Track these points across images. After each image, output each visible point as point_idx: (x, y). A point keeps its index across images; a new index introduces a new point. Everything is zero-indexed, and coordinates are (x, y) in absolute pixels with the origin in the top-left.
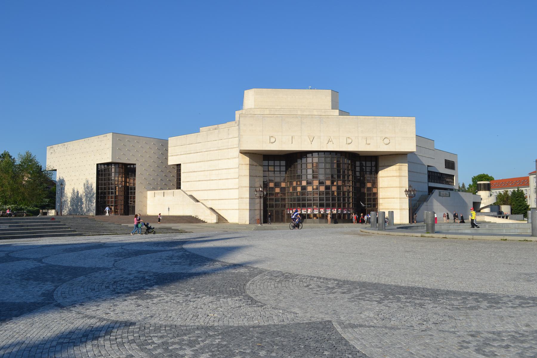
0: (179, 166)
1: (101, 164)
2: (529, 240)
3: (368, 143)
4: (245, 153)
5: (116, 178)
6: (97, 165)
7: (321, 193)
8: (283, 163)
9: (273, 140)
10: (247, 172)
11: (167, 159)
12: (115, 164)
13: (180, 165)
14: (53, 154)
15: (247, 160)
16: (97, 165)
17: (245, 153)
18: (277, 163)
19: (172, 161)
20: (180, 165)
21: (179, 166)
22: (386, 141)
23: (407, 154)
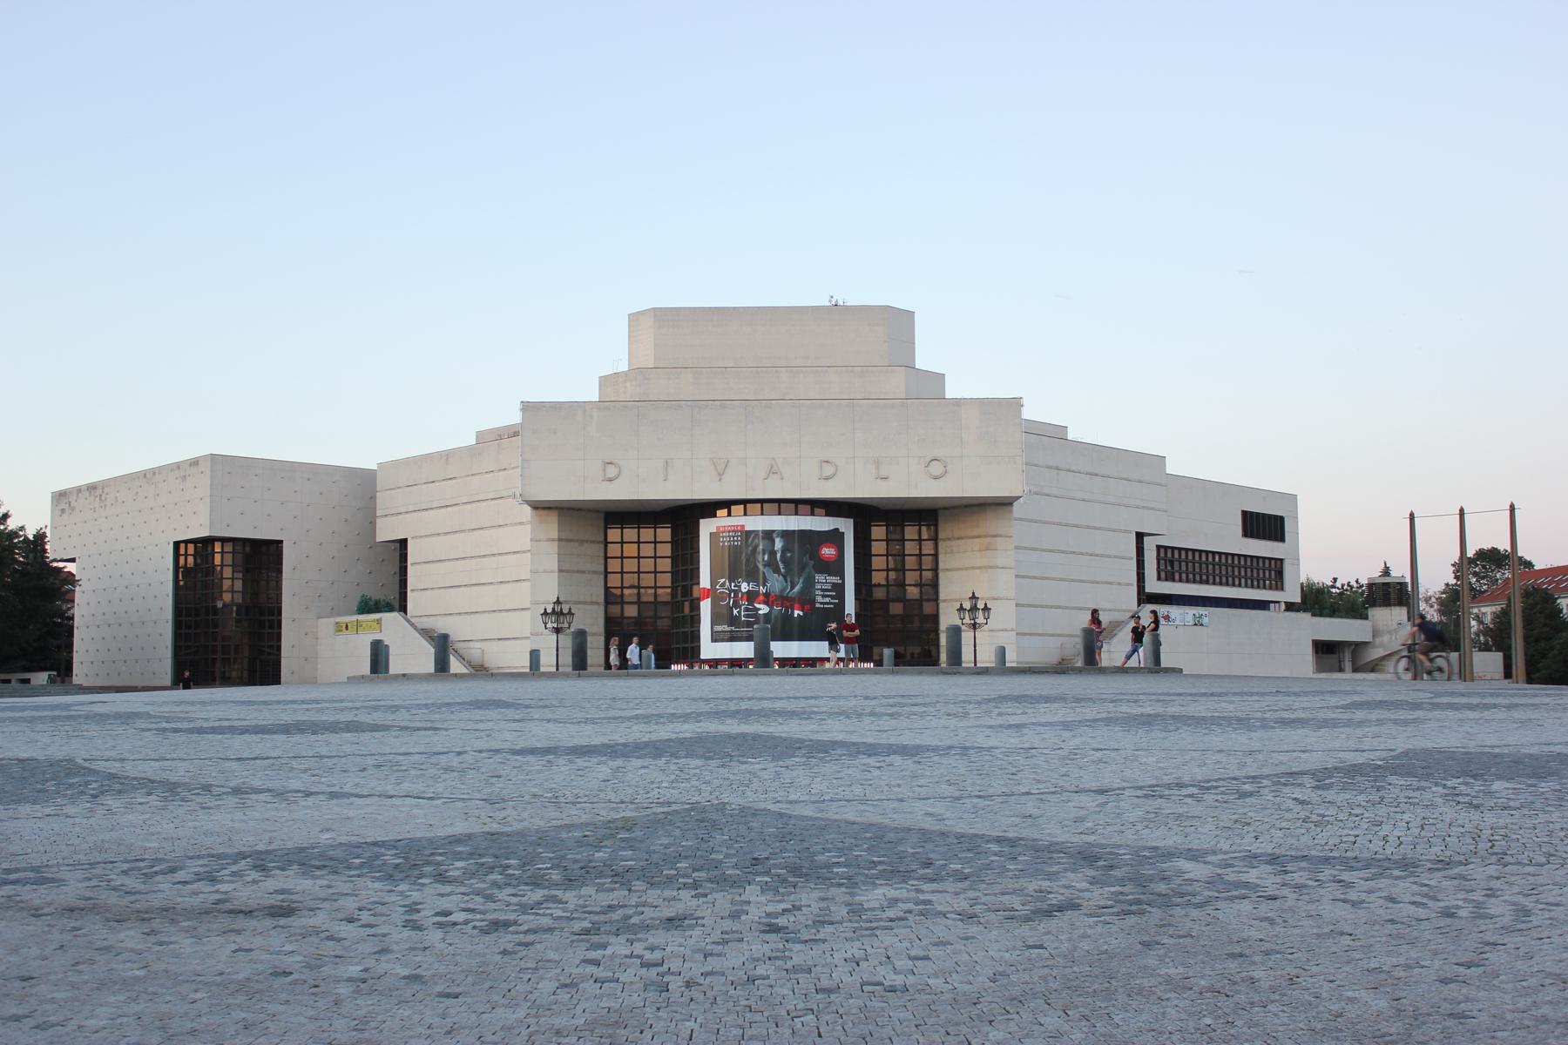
0: (403, 543)
1: (187, 542)
2: (701, 703)
3: (883, 473)
4: (539, 507)
5: (231, 587)
6: (177, 544)
7: (214, 600)
8: (665, 533)
9: (612, 471)
10: (553, 563)
11: (373, 524)
12: (224, 540)
13: (405, 541)
14: (65, 516)
15: (552, 527)
16: (177, 544)
17: (539, 507)
18: (647, 534)
19: (387, 531)
20: (405, 541)
21: (403, 543)
22: (936, 469)
23: (1011, 504)
